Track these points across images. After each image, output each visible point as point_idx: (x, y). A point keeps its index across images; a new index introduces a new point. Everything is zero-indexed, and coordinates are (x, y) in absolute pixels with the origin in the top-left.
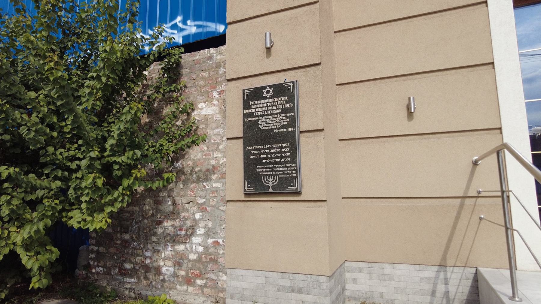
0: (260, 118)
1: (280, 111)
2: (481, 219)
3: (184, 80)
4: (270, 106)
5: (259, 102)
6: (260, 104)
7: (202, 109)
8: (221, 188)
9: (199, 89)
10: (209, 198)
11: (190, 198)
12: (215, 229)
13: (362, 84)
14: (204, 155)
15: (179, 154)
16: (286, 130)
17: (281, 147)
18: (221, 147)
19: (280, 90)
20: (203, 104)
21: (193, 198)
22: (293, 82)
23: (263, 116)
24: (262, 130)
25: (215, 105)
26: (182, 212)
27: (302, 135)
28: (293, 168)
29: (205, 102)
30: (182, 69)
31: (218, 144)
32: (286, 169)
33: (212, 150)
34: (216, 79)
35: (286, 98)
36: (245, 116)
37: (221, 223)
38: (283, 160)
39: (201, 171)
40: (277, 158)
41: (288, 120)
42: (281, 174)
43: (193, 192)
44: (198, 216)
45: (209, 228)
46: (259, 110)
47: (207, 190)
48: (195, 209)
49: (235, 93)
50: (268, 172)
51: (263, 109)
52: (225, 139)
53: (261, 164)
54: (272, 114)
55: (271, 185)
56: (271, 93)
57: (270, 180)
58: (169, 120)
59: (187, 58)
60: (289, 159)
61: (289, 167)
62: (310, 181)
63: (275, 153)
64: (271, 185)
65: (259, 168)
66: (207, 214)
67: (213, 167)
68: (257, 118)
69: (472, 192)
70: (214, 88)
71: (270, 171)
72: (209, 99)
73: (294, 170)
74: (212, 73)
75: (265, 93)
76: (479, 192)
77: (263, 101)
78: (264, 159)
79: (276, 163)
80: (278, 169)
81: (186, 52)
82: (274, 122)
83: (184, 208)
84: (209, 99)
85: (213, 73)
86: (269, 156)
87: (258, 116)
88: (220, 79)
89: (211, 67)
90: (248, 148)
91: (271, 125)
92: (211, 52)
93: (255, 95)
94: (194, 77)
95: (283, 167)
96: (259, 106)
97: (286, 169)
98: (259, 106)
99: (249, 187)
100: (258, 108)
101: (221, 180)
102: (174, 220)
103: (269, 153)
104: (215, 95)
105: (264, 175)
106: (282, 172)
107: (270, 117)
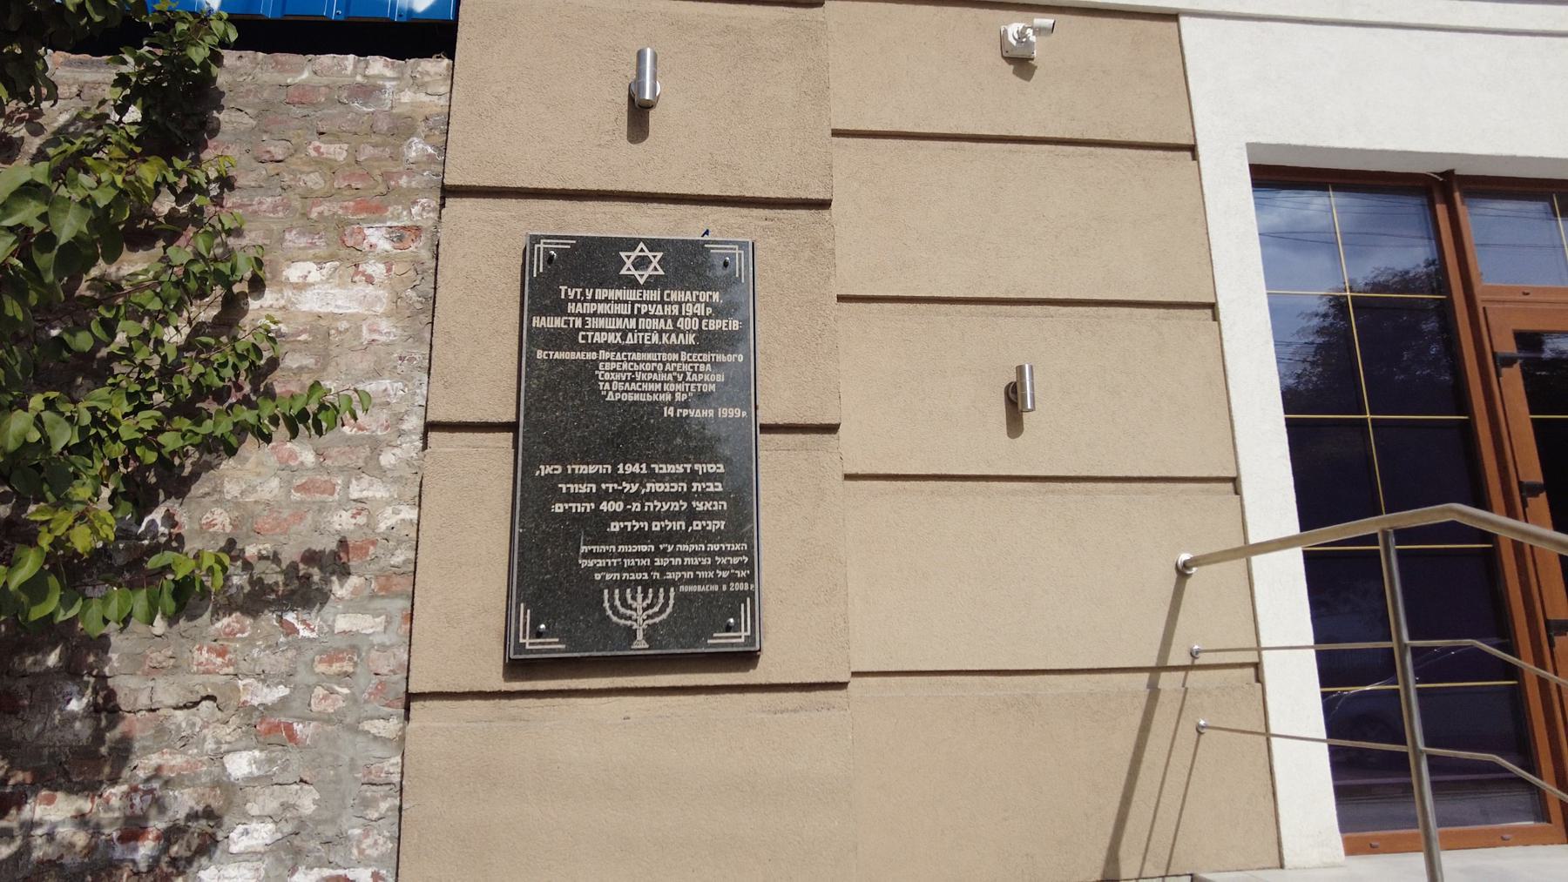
0: (604, 355)
1: (691, 339)
2: (1199, 730)
3: (217, 156)
4: (647, 315)
5: (601, 293)
6: (607, 301)
7: (302, 286)
8: (376, 640)
9: (297, 204)
10: (312, 680)
11: (200, 684)
12: (333, 821)
13: (875, 306)
14: (300, 488)
15: (154, 481)
16: (711, 413)
17: (692, 477)
18: (387, 459)
19: (687, 264)
20: (312, 266)
21: (220, 679)
22: (742, 245)
23: (619, 348)
24: (612, 404)
25: (370, 280)
26: (147, 750)
27: (509, 416)
28: (735, 561)
29: (320, 261)
30: (220, 108)
31: (376, 446)
32: (706, 561)
33: (341, 470)
34: (387, 176)
35: (716, 296)
36: (531, 339)
37: (369, 792)
38: (697, 525)
39: (275, 558)
40: (673, 516)
41: (720, 378)
42: (689, 582)
43: (222, 653)
44: (240, 765)
45: (302, 822)
46: (601, 323)
47: (299, 646)
48: (227, 733)
49: (487, 254)
50: (630, 569)
51: (619, 323)
52: (414, 423)
53: (606, 538)
54: (654, 348)
55: (640, 629)
56: (655, 269)
57: (639, 603)
58: (156, 305)
59: (241, 72)
60: (721, 524)
61: (721, 553)
62: (787, 638)
63: (664, 497)
64: (640, 629)
65: (587, 556)
66: (294, 756)
67: (343, 543)
68: (592, 356)
69: (1178, 657)
70: (374, 210)
71: (640, 569)
72: (343, 252)
73: (740, 566)
74: (367, 152)
75: (629, 263)
76: (1194, 655)
77: (619, 294)
78: (615, 516)
79: (670, 536)
80: (677, 561)
81: (239, 46)
82: (663, 377)
83: (161, 731)
84: (344, 252)
85: (377, 152)
86: (636, 507)
87: (596, 347)
88: (403, 181)
89: (366, 127)
90: (545, 470)
91: (651, 387)
92: (370, 72)
93: (591, 262)
94: (278, 151)
95: (694, 554)
96: (602, 308)
97: (706, 561)
98: (602, 308)
99: (539, 635)
100: (595, 315)
101: (378, 604)
102: (90, 788)
103: (636, 496)
104: (377, 237)
105: (611, 585)
106: (689, 575)
107: (649, 356)
